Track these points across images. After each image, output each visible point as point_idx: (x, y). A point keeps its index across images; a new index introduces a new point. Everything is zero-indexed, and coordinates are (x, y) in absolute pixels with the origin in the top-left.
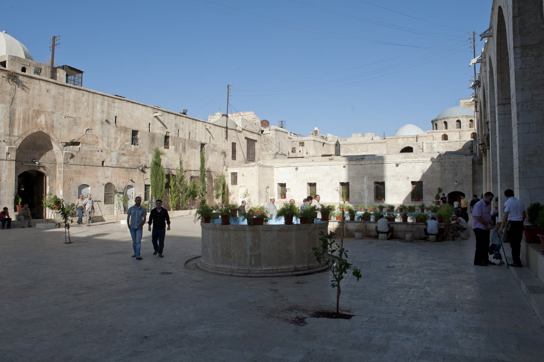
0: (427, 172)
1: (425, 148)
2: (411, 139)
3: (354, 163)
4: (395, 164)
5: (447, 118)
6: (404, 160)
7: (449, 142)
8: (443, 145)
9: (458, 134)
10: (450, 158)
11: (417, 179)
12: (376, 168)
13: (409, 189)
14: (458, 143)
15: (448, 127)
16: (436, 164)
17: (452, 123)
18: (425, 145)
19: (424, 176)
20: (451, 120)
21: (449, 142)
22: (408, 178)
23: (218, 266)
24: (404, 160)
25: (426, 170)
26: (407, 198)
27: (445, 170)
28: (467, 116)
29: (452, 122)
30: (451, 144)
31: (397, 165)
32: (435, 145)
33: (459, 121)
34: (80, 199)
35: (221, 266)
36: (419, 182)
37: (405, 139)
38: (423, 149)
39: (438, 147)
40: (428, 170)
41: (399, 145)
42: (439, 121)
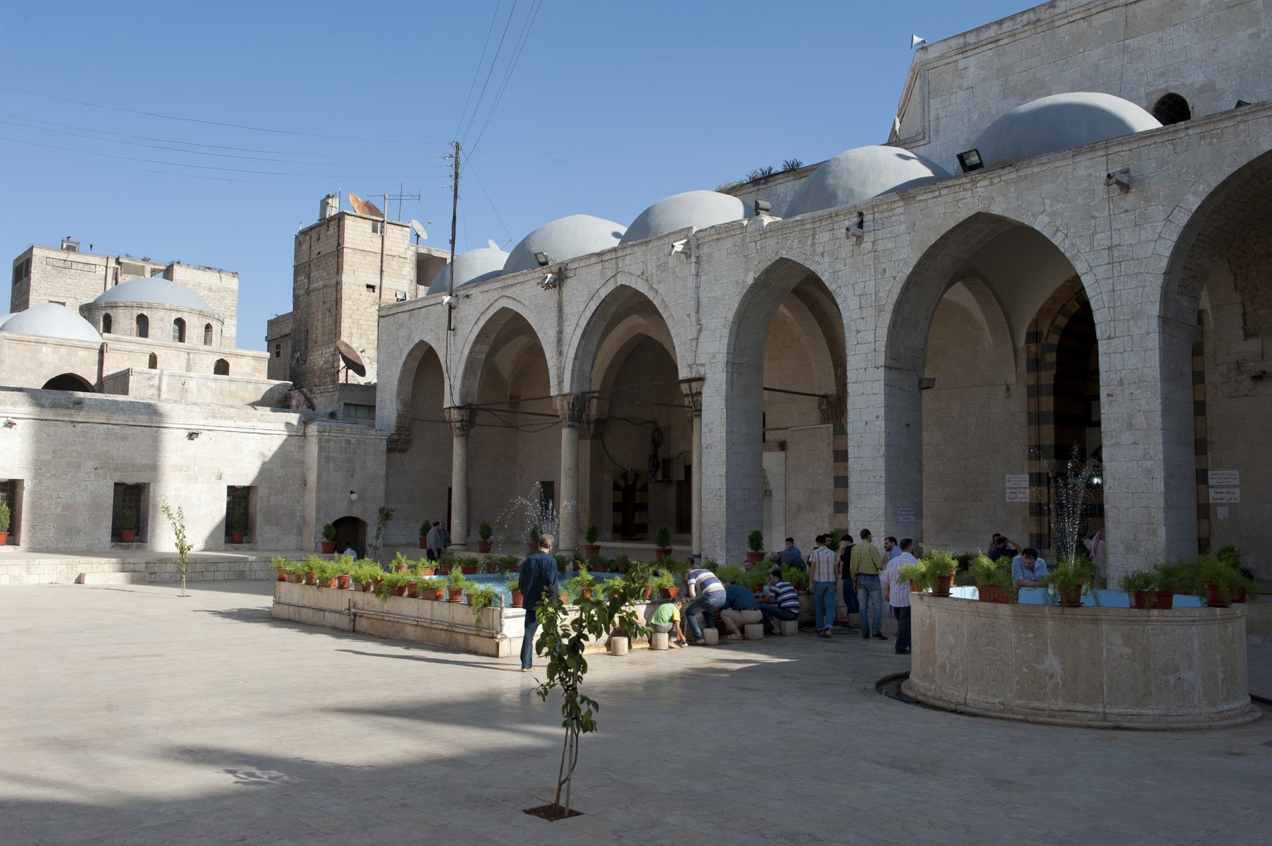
0: (271, 461)
1: (164, 387)
2: (82, 353)
3: (49, 414)
4: (186, 433)
5: (150, 307)
6: (212, 423)
7: (231, 381)
8: (213, 385)
9: (184, 355)
10: (342, 431)
11: (245, 480)
12: (124, 438)
13: (217, 509)
14: (251, 387)
15: (187, 333)
16: (294, 441)
17: (161, 326)
18: (165, 380)
19: (266, 470)
20: (161, 314)
21: (231, 381)
22: (220, 477)
23: (1221, 709)
24: (212, 423)
25: (269, 454)
26: (213, 535)
27: (328, 459)
28: (201, 314)
29: (162, 320)
30: (233, 387)
31: (192, 436)
32: (192, 384)
33: (180, 323)
34: (457, 572)
35: (1226, 707)
36: (245, 488)
37: (64, 350)
38: (159, 389)
39: (199, 391)
40: (274, 456)
41: (40, 365)
42: (120, 311)
